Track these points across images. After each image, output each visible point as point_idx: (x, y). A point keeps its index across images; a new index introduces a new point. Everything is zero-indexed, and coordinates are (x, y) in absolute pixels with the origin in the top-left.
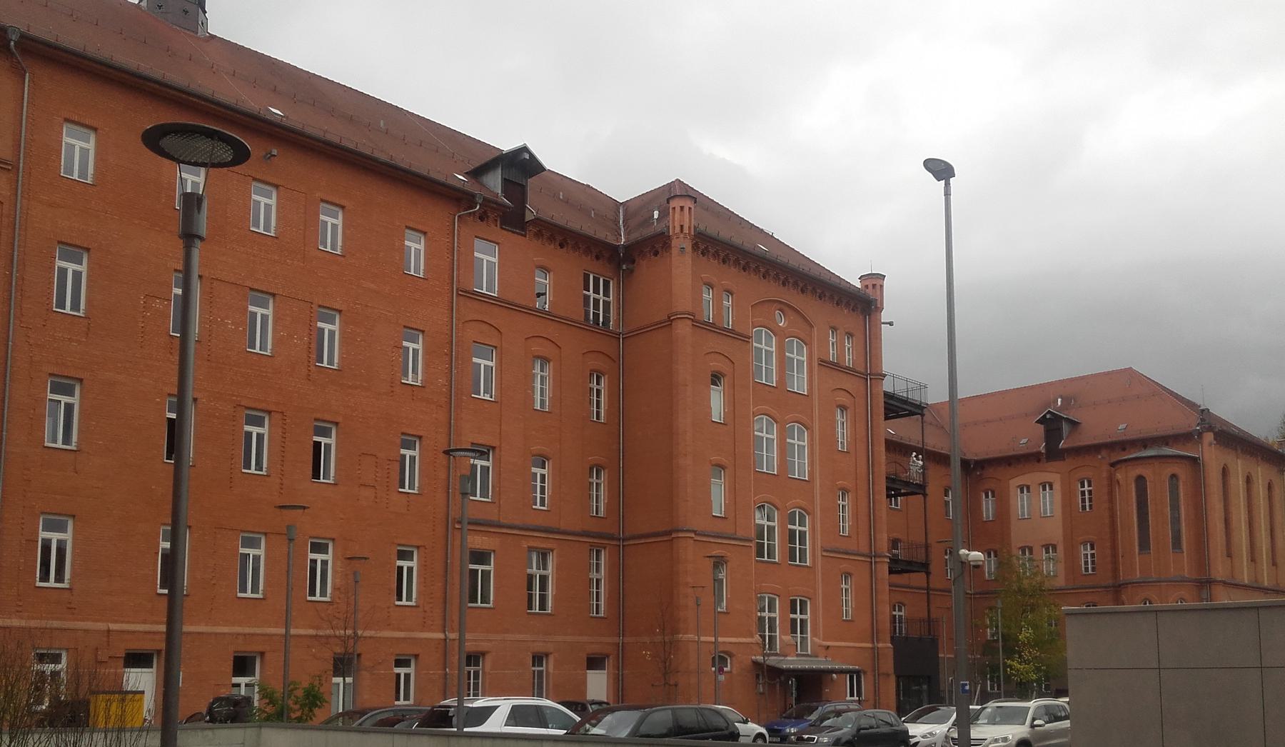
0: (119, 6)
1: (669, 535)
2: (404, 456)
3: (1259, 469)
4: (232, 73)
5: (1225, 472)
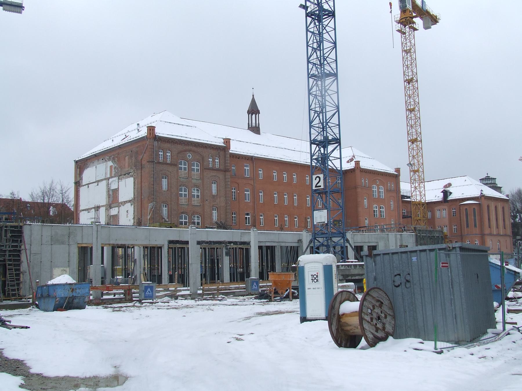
0: (497, 355)
1: (356, 188)
2: (259, 173)
3: (499, 204)
4: (404, 244)
5: (488, 206)
